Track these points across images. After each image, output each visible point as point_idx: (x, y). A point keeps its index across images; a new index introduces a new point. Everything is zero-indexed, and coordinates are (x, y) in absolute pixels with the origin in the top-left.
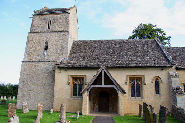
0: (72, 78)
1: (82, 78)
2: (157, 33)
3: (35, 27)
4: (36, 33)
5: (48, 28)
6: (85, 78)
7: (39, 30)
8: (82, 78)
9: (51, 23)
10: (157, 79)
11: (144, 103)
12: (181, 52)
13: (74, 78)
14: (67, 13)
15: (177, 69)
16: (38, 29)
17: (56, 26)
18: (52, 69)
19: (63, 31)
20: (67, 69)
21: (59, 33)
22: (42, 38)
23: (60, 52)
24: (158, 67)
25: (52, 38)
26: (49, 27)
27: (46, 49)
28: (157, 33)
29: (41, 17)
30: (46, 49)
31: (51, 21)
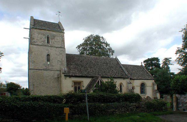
0: (74, 82)
1: (80, 83)
2: (102, 44)
3: (35, 40)
4: (38, 45)
5: (48, 43)
6: (82, 83)
7: (40, 44)
8: (80, 83)
9: (50, 40)
10: (121, 84)
11: (176, 53)
12: (87, 55)
13: (75, 83)
14: (63, 32)
15: (131, 79)
16: (38, 42)
17: (55, 42)
18: (56, 76)
19: (61, 48)
20: (70, 77)
21: (58, 48)
22: (44, 51)
23: (60, 63)
24: (122, 78)
25: (53, 52)
26: (48, 42)
27: (48, 60)
28: (102, 44)
29: (38, 30)
30: (48, 60)
31: (49, 37)
